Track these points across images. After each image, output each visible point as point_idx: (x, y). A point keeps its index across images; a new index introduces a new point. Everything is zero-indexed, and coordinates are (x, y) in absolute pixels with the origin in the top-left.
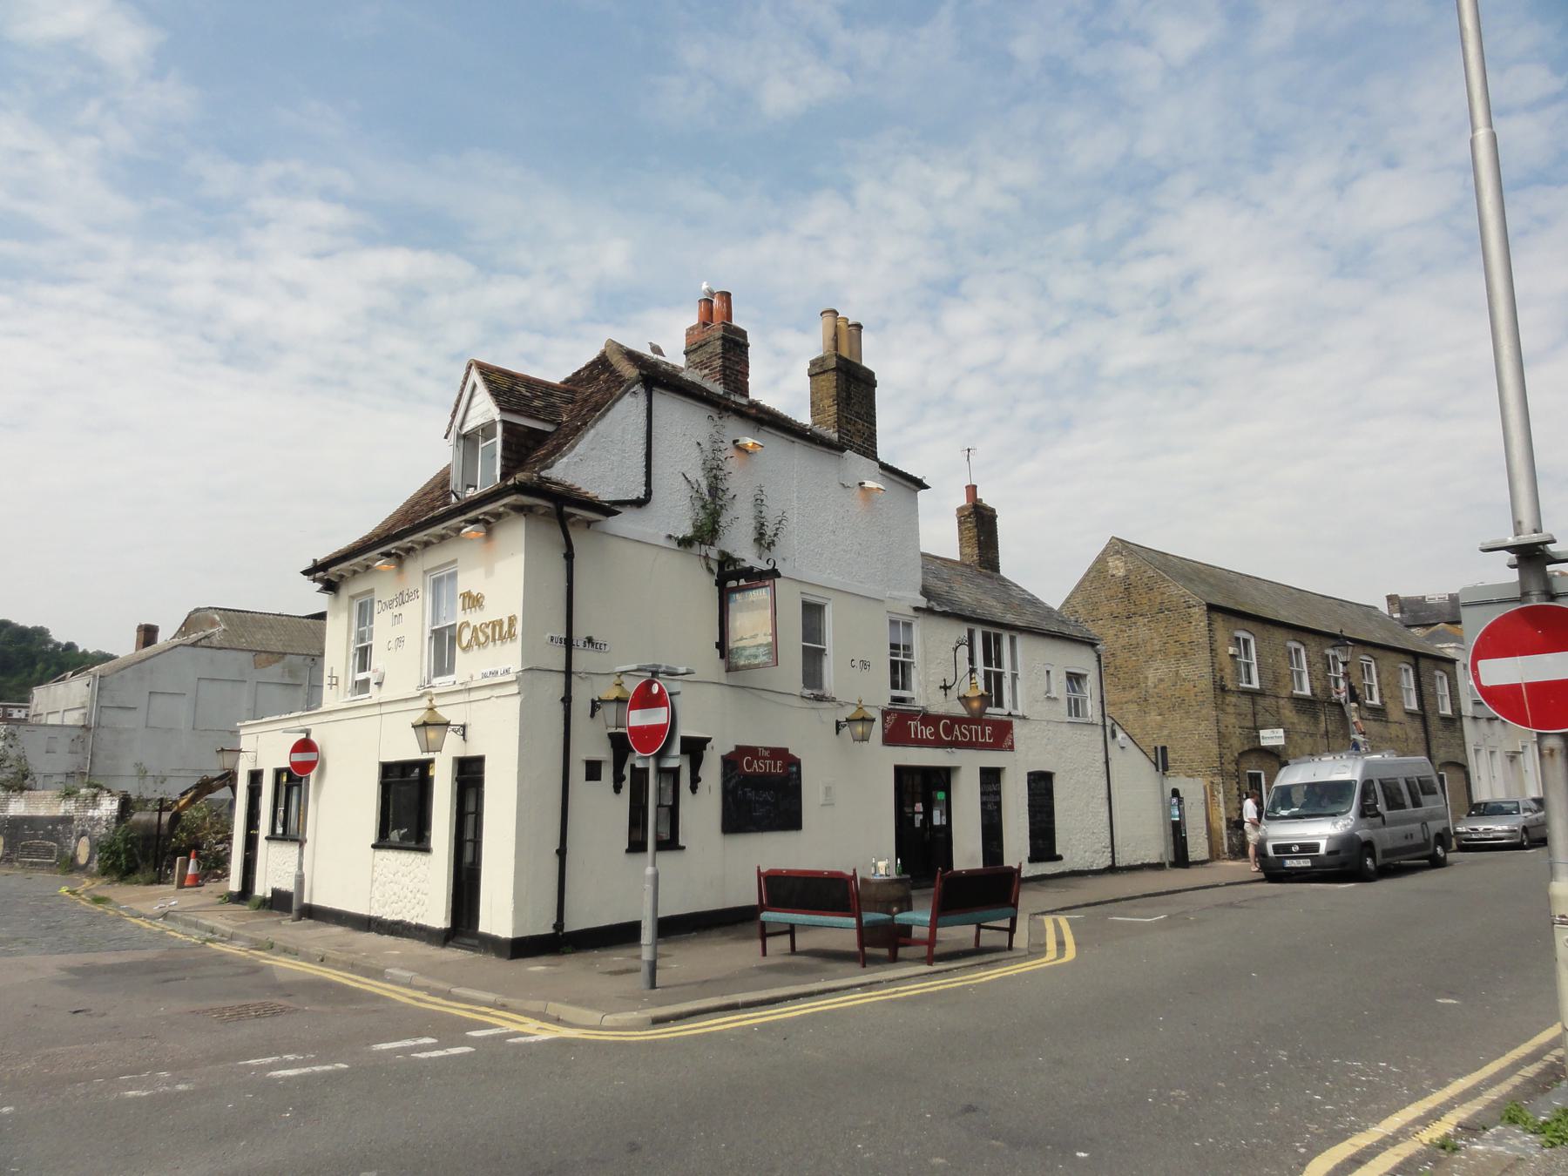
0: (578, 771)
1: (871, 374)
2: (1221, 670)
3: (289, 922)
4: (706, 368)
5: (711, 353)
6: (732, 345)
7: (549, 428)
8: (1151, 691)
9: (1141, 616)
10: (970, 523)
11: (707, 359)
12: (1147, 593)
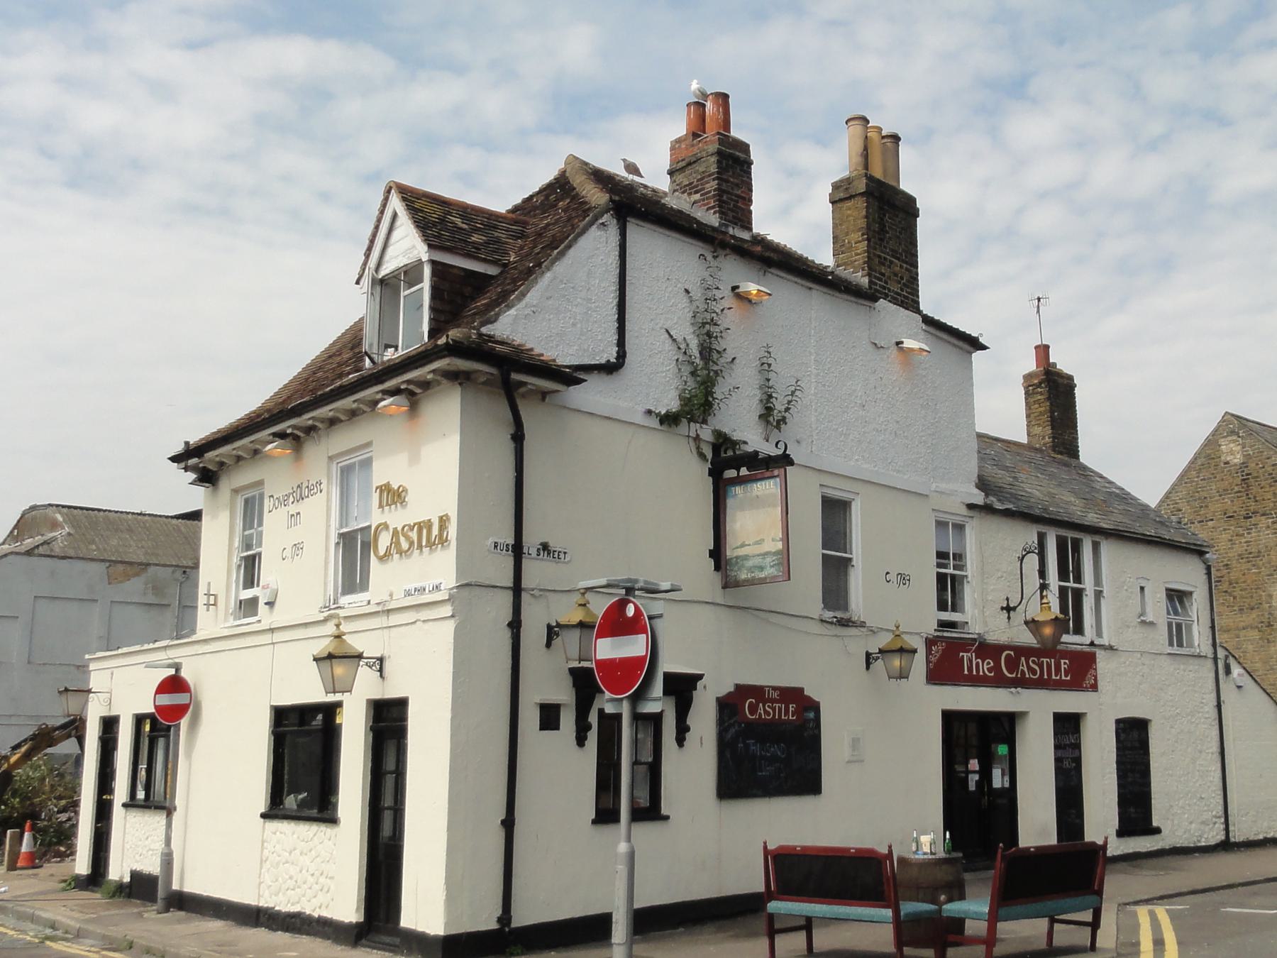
0: (530, 717)
1: (911, 201)
3: (153, 915)
4: (696, 192)
7: (492, 271)
9: (1263, 515)
10: (1041, 393)
12: (1271, 486)
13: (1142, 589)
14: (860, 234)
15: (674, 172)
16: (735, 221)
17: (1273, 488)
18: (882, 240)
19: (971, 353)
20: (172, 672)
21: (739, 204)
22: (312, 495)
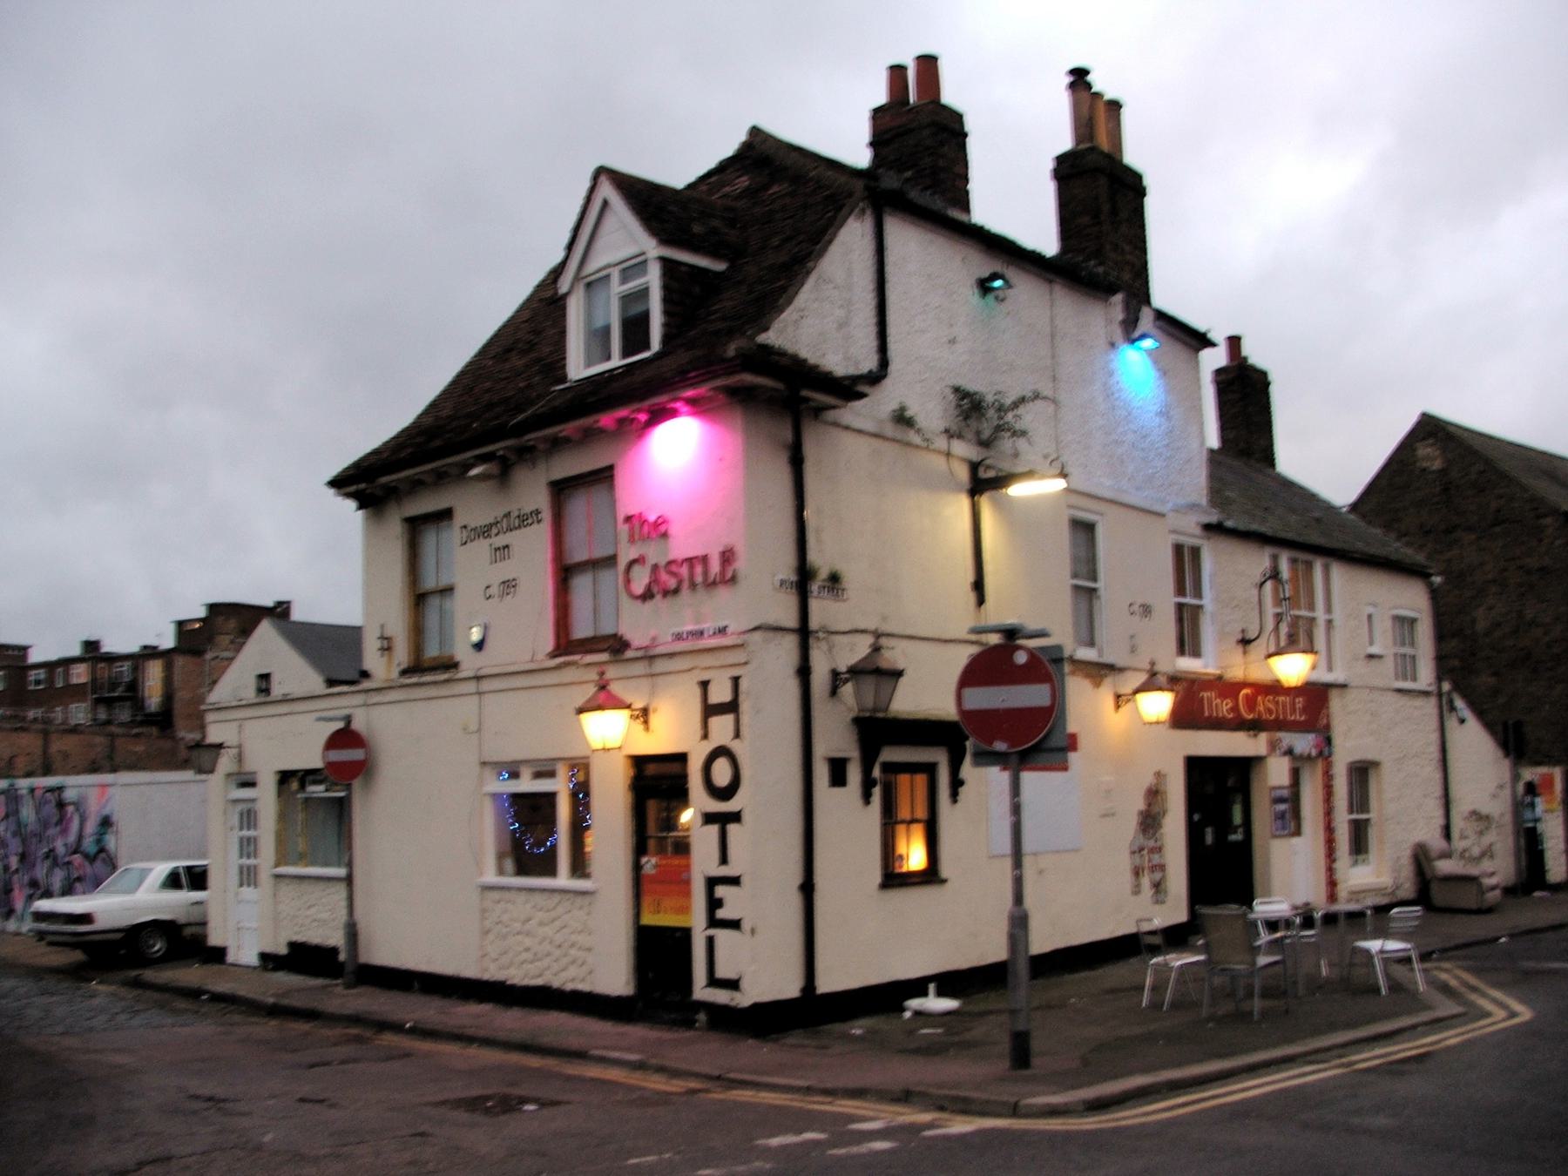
0: (821, 773)
3: (339, 989)
4: (908, 169)
7: (720, 266)
13: (1370, 617)
20: (340, 725)
22: (525, 526)
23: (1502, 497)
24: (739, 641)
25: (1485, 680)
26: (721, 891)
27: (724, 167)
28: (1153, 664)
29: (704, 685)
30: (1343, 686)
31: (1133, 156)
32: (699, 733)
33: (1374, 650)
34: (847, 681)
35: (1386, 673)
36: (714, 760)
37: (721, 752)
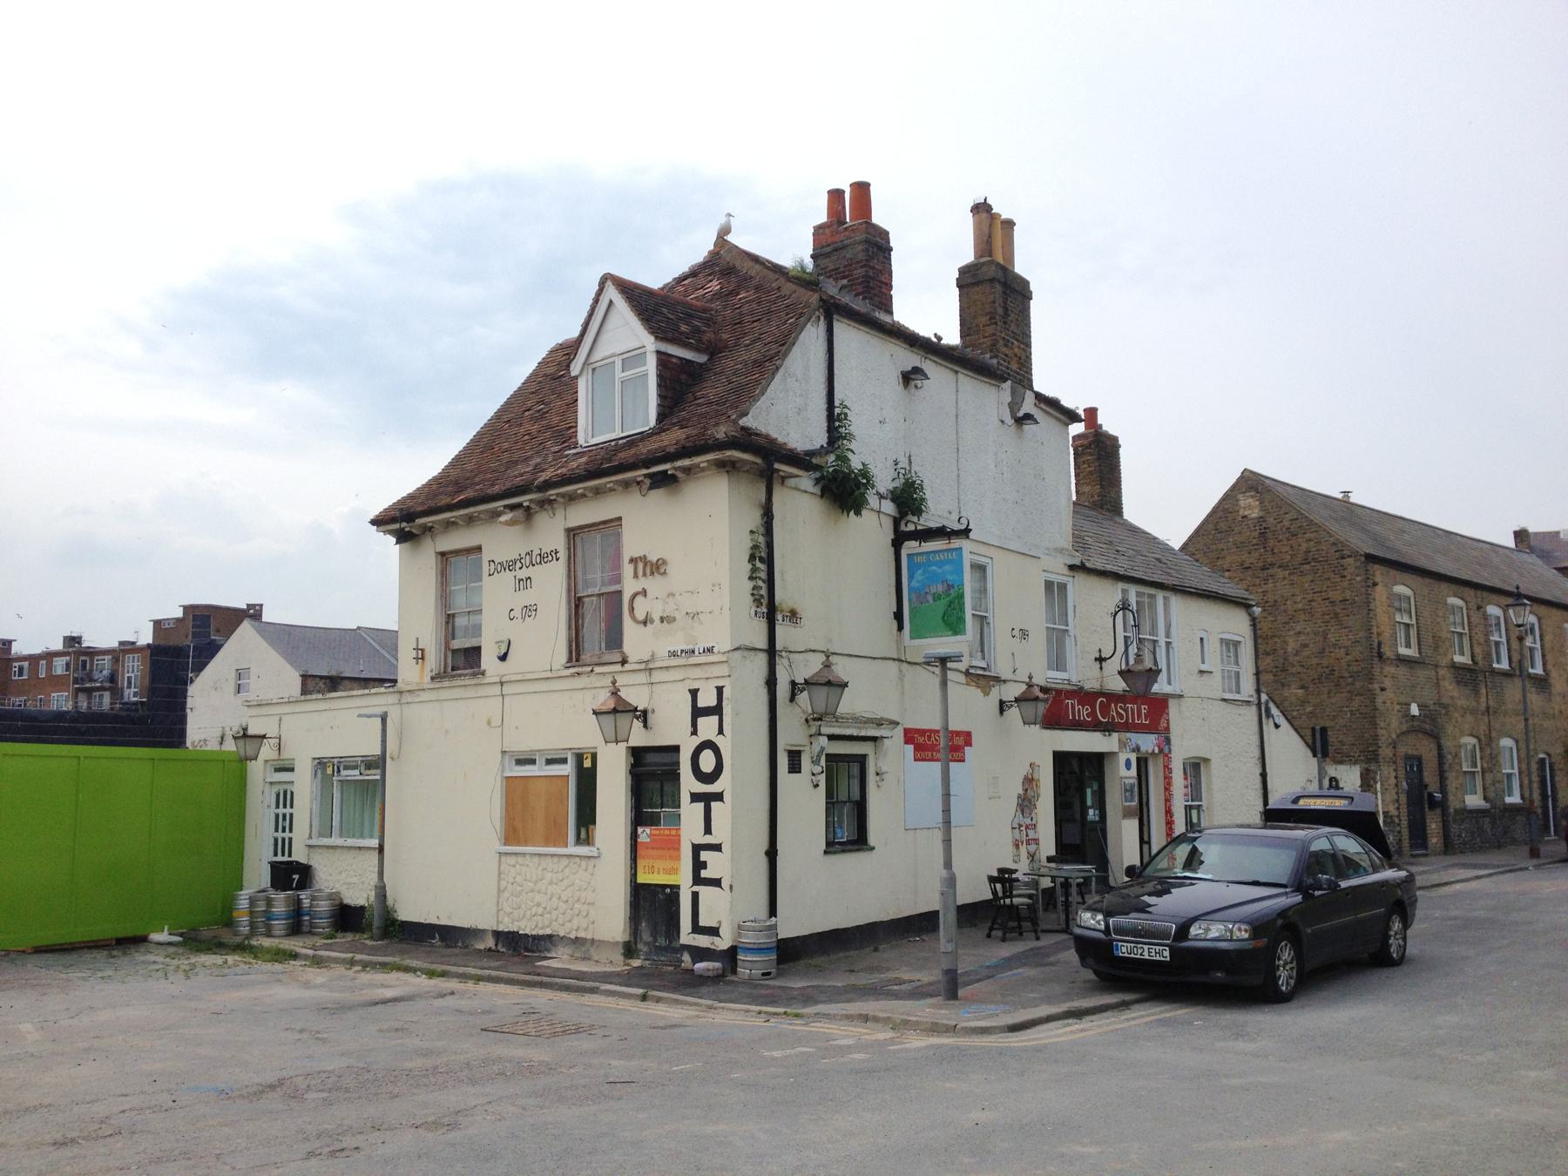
1: (1024, 284)
2: (1379, 634)
4: (844, 277)
5: (851, 259)
6: (875, 250)
7: (701, 358)
8: (1291, 658)
9: (1280, 567)
10: (1091, 454)
11: (845, 267)
12: (1288, 540)
14: (988, 317)
15: (818, 256)
16: (880, 306)
17: (1291, 542)
18: (1005, 323)
19: (1067, 425)
21: (883, 290)
23: (1310, 540)
24: (724, 659)
25: (1294, 692)
26: (704, 855)
27: (694, 273)
28: (1030, 678)
29: (694, 693)
30: (1181, 696)
31: (1020, 268)
32: (690, 729)
33: (1204, 667)
34: (804, 689)
35: (1215, 686)
36: (702, 751)
37: (708, 744)
